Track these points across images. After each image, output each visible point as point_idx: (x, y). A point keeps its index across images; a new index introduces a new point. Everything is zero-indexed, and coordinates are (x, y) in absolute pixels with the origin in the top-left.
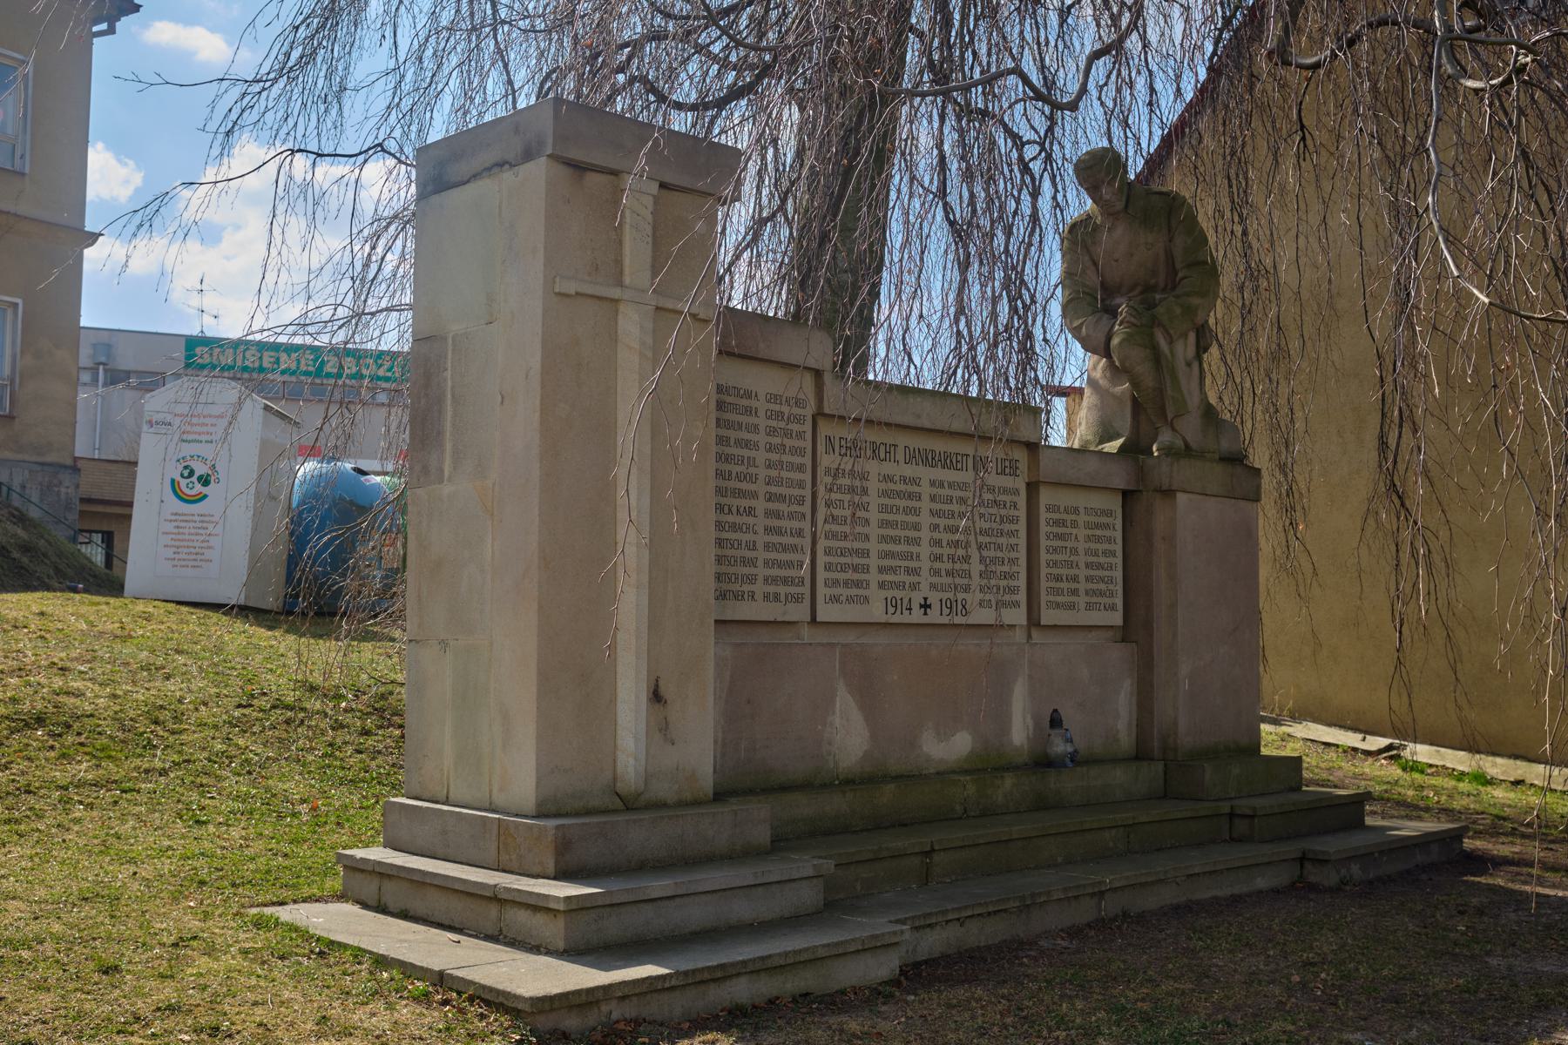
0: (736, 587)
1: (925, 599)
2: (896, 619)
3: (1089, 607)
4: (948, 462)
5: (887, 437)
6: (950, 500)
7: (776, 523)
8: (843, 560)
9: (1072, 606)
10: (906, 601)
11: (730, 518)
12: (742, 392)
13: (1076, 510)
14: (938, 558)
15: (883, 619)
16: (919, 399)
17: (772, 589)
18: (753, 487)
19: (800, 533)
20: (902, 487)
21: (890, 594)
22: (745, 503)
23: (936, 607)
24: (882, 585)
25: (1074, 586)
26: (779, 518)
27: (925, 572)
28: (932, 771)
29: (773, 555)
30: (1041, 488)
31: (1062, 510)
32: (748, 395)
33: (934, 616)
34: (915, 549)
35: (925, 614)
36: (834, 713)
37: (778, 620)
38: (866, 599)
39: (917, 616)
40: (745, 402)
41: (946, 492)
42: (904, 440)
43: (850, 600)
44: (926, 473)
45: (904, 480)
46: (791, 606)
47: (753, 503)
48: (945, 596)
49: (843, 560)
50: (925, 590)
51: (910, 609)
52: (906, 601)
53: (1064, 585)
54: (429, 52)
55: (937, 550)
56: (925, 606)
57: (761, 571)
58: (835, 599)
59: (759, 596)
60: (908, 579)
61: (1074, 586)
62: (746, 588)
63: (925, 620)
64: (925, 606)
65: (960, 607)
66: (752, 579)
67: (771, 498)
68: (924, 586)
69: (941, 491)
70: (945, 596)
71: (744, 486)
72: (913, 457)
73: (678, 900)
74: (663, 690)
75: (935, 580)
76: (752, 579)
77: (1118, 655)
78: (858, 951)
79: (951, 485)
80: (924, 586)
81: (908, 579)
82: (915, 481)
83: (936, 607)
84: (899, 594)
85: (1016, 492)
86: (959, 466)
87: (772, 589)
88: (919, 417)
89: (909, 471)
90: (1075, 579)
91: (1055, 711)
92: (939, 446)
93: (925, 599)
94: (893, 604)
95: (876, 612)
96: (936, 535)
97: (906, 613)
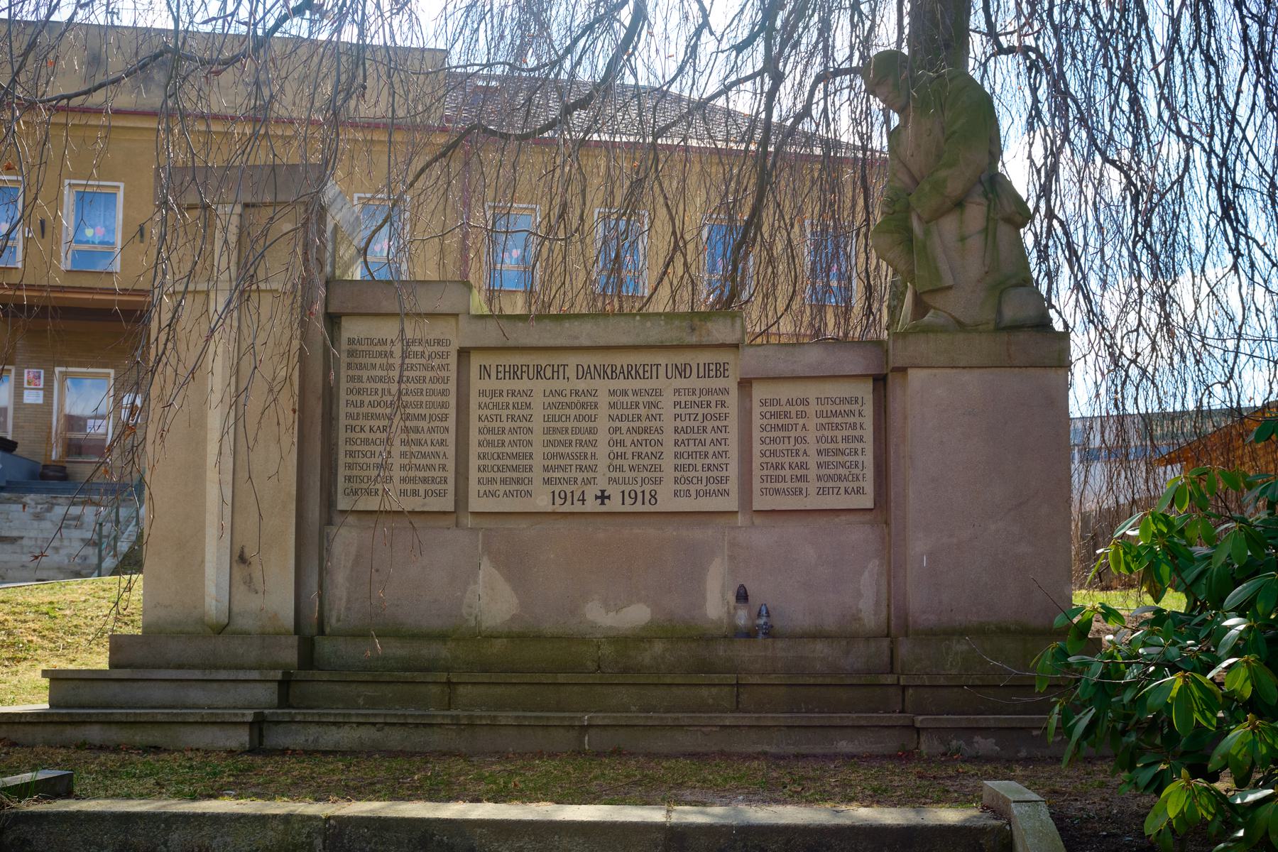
3: (821, 491)
5: (557, 360)
12: (375, 341)
13: (804, 401)
15: (550, 509)
16: (567, 325)
20: (574, 399)
30: (754, 385)
36: (476, 583)
37: (417, 510)
39: (592, 505)
42: (572, 360)
44: (603, 385)
50: (602, 483)
51: (583, 500)
56: (603, 497)
64: (603, 497)
72: (583, 373)
73: (141, 683)
74: (248, 554)
77: (859, 535)
78: (196, 723)
79: (635, 393)
82: (593, 393)
85: (726, 391)
86: (646, 375)
88: (577, 338)
89: (582, 385)
91: (742, 586)
92: (621, 360)
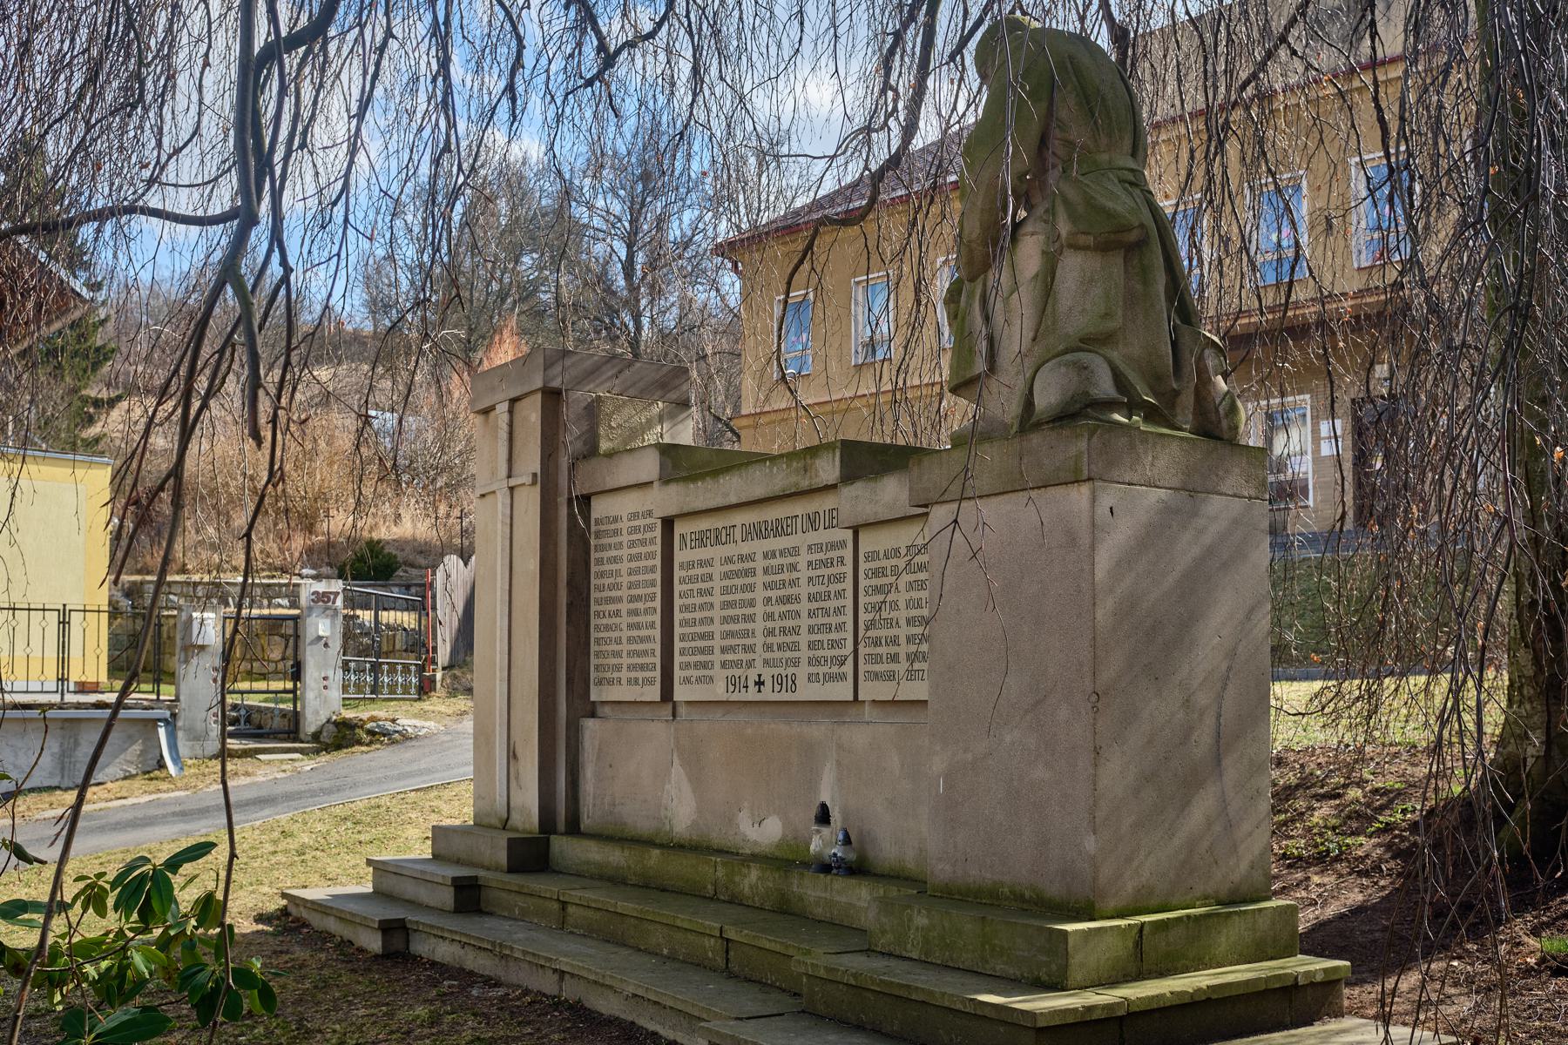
0: (608, 675)
1: (760, 676)
2: (735, 697)
4: (779, 529)
6: (781, 569)
7: (636, 619)
8: (693, 644)
9: (891, 676)
10: (743, 679)
11: (604, 621)
14: (771, 632)
17: (633, 675)
18: (619, 593)
19: (839, 611)
21: (730, 672)
22: (612, 607)
23: (768, 683)
24: (724, 665)
25: (893, 650)
26: (637, 615)
27: (759, 649)
28: (748, 851)
29: (634, 647)
31: (881, 555)
32: (616, 520)
33: (767, 694)
34: (749, 626)
35: (759, 691)
38: (711, 679)
39: (752, 694)
40: (613, 527)
41: (778, 561)
43: (699, 680)
44: (759, 546)
45: (742, 558)
46: (647, 688)
47: (619, 606)
48: (776, 671)
49: (693, 644)
52: (743, 679)
53: (882, 650)
54: (631, 325)
55: (770, 624)
56: (760, 683)
57: (626, 661)
58: (687, 680)
59: (624, 681)
60: (745, 657)
61: (893, 650)
62: (615, 675)
63: (759, 697)
64: (760, 683)
65: (790, 682)
66: (618, 668)
67: (633, 599)
68: (759, 663)
69: (774, 562)
70: (776, 671)
71: (614, 594)
75: (768, 655)
76: (618, 668)
80: (759, 663)
81: (745, 657)
83: (768, 683)
84: (737, 672)
87: (633, 675)
89: (745, 548)
90: (894, 641)
93: (760, 676)
94: (733, 682)
95: (719, 691)
96: (769, 609)
97: (743, 690)
